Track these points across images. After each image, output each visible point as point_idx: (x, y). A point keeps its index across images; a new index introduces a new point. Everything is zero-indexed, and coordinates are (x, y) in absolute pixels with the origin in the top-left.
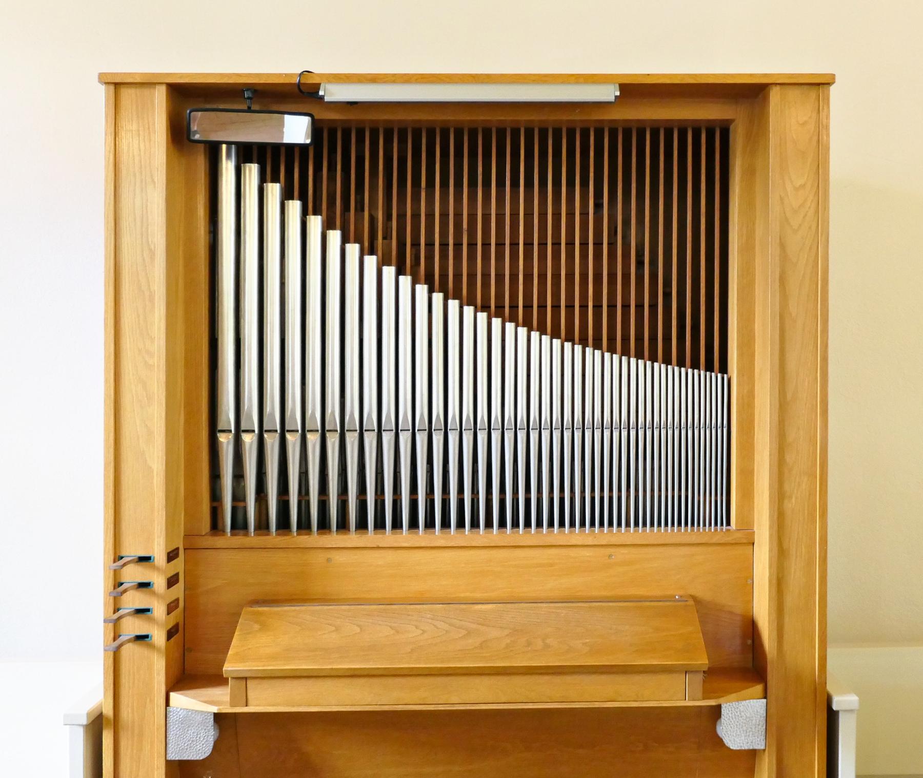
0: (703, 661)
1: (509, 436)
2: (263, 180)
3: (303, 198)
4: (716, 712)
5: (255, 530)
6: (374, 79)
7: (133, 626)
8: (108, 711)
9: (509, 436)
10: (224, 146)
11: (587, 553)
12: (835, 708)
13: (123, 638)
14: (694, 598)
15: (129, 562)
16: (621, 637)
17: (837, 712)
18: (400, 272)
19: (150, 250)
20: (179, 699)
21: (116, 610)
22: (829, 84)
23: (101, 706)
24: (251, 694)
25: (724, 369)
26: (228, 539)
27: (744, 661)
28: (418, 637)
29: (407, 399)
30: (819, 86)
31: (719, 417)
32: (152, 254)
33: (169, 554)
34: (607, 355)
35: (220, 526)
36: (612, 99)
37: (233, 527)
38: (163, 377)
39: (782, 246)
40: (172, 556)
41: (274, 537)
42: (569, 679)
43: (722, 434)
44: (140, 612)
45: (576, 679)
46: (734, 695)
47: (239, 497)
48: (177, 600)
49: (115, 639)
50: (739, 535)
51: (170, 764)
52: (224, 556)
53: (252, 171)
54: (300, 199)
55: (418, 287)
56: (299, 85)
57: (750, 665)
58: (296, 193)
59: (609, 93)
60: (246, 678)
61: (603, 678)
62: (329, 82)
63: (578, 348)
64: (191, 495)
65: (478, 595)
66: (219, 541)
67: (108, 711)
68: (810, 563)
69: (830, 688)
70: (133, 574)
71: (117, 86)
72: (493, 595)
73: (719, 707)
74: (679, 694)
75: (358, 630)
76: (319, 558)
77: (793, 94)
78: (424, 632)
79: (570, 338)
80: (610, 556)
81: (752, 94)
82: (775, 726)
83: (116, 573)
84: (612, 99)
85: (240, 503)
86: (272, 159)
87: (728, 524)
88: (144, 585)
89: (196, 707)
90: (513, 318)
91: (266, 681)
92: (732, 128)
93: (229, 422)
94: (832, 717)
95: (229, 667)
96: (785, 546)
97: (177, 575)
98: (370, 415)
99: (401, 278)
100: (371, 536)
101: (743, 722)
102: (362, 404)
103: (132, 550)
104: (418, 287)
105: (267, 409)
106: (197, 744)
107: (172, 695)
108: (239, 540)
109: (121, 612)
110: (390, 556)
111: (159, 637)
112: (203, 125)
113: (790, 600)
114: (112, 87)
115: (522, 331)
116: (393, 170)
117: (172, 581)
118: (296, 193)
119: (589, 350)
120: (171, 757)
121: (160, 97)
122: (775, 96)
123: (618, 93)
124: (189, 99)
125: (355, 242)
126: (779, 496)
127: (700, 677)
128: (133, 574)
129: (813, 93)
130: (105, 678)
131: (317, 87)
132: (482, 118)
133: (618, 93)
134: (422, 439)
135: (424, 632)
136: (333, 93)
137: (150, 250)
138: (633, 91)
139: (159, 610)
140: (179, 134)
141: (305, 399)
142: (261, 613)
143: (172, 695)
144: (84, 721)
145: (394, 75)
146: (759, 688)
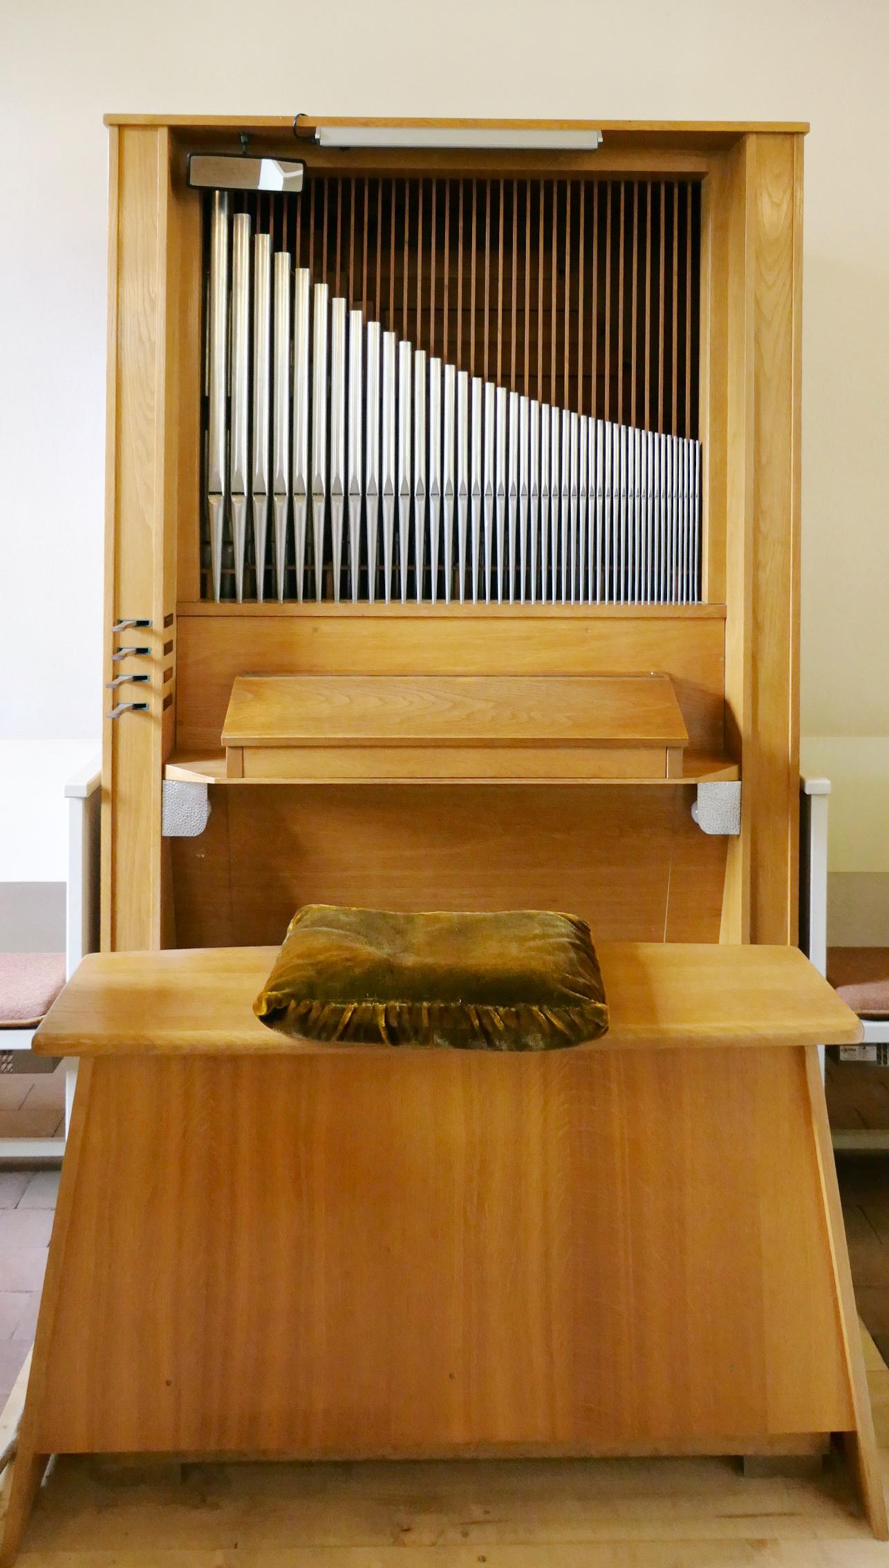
0: (683, 736)
1: (488, 503)
2: (253, 232)
3: (291, 250)
4: (691, 793)
5: (244, 597)
6: (366, 123)
7: (131, 695)
8: (107, 784)
9: (488, 503)
10: (217, 192)
11: (563, 625)
12: (807, 792)
13: (122, 707)
14: (670, 675)
15: (126, 627)
16: (601, 712)
17: (809, 796)
18: (384, 328)
19: (151, 299)
20: (173, 771)
21: (115, 677)
22: (803, 133)
23: (99, 778)
24: (248, 765)
25: (695, 435)
26: (217, 605)
27: (719, 741)
28: (403, 708)
29: (389, 464)
30: (792, 135)
31: (691, 486)
32: (153, 302)
33: (165, 618)
34: (583, 418)
35: (209, 595)
36: (595, 146)
37: (222, 596)
38: (162, 432)
39: (758, 303)
40: (168, 621)
41: (261, 605)
42: (553, 753)
43: (694, 504)
44: (139, 679)
45: (561, 753)
46: (712, 775)
47: (228, 563)
48: (171, 669)
49: (113, 708)
50: (711, 609)
51: (164, 839)
52: (216, 624)
53: (244, 221)
54: (288, 251)
55: (402, 343)
56: (295, 128)
57: (722, 747)
58: (285, 246)
59: (591, 140)
60: (242, 748)
61: (587, 752)
62: (324, 125)
63: (555, 410)
64: (183, 562)
65: (459, 669)
66: (209, 608)
67: (107, 784)
68: (784, 638)
69: (803, 773)
70: (132, 639)
71: (121, 127)
72: (472, 669)
73: (694, 788)
74: (656, 771)
75: (347, 700)
76: (305, 627)
77: (769, 142)
78: (411, 703)
79: (546, 399)
80: (587, 629)
81: (724, 144)
82: (751, 809)
83: (115, 635)
84: (595, 146)
85: (236, 569)
86: (263, 209)
87: (700, 599)
88: (142, 651)
89: (191, 778)
90: (492, 378)
91: (260, 751)
92: (704, 182)
93: (241, 477)
94: (805, 800)
95: (228, 735)
96: (760, 618)
97: (171, 642)
98: (355, 477)
99: (386, 334)
100: (354, 606)
101: (718, 804)
102: (348, 468)
103: (131, 614)
104: (402, 343)
105: (256, 470)
106: (191, 819)
107: (168, 767)
108: (228, 607)
109: (121, 679)
110: (372, 626)
111: (155, 706)
112: (204, 171)
113: (764, 677)
114: (116, 130)
115: (501, 392)
116: (381, 220)
117: (167, 648)
118: (285, 246)
119: (565, 413)
120: (167, 833)
121: (161, 140)
122: (751, 145)
123: (601, 140)
124: (190, 140)
125: (341, 296)
126: (755, 565)
127: (679, 755)
128: (132, 639)
129: (787, 144)
130: (104, 748)
131: (312, 130)
132: (489, 168)
133: (601, 140)
134: (404, 504)
135: (411, 703)
136: (329, 137)
137: (151, 299)
138: (618, 139)
139: (156, 678)
140: (179, 181)
141: (296, 463)
142: (253, 683)
143: (168, 767)
144: (85, 794)
145: (386, 119)
146: (733, 769)
